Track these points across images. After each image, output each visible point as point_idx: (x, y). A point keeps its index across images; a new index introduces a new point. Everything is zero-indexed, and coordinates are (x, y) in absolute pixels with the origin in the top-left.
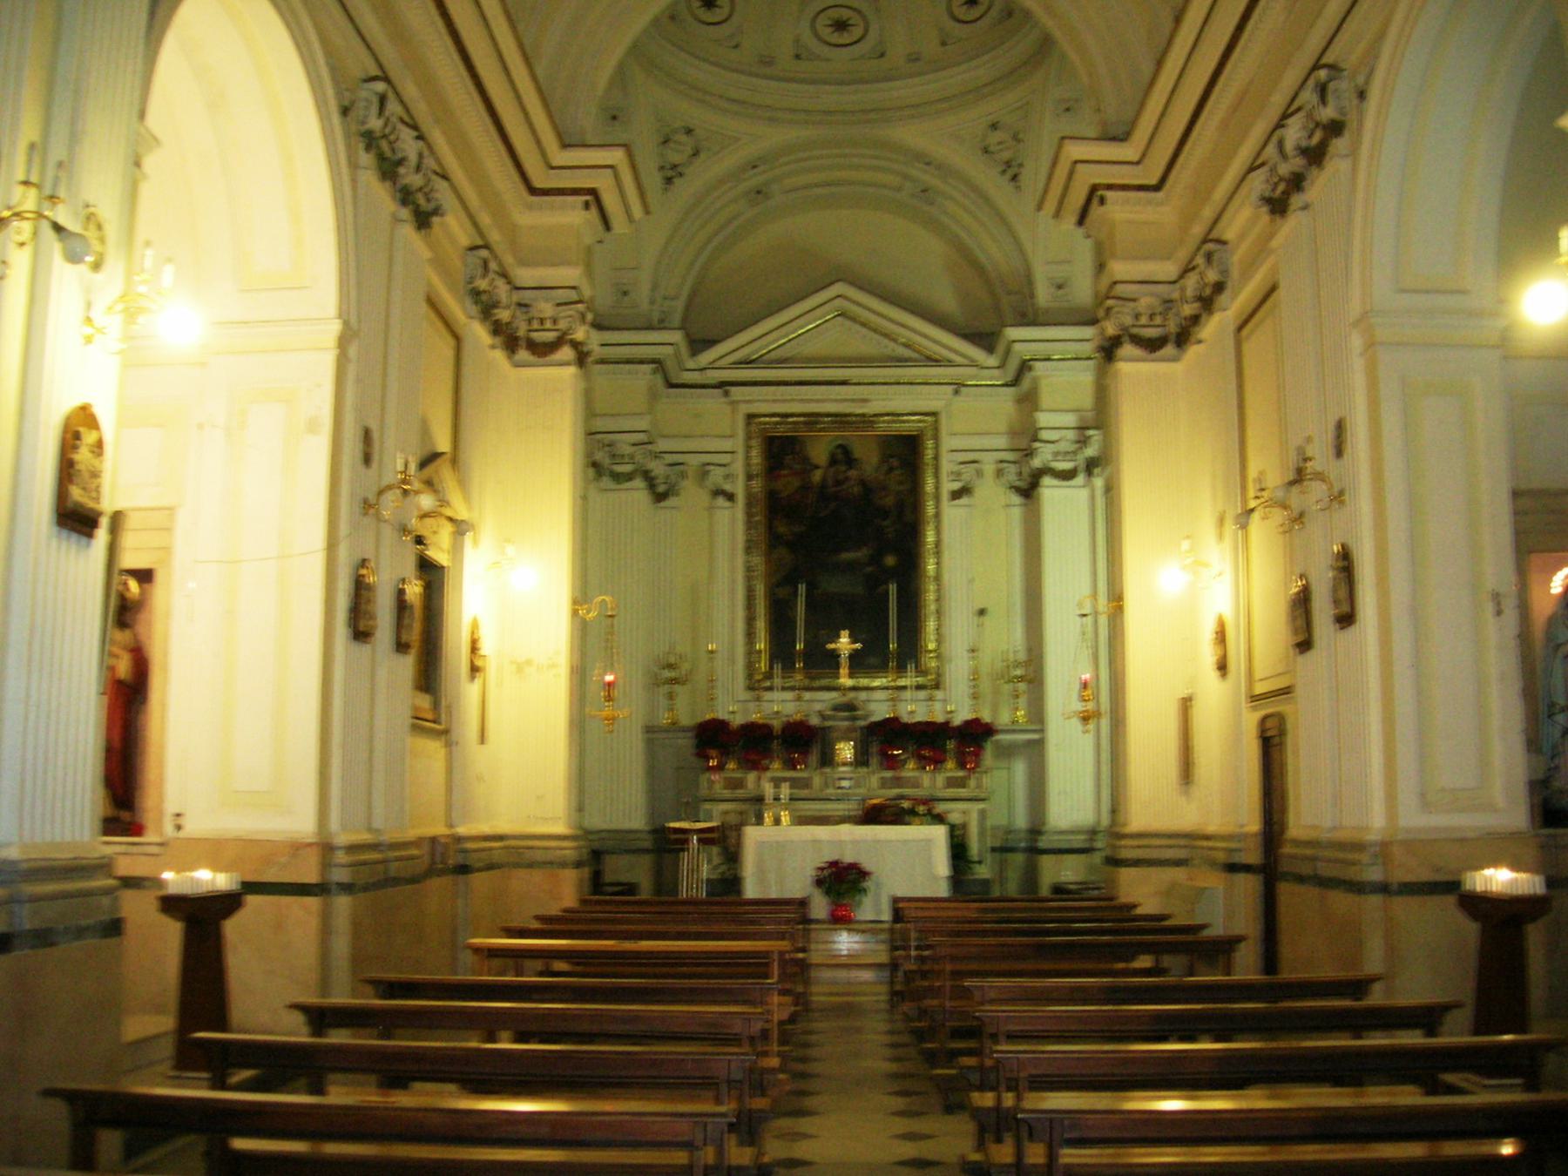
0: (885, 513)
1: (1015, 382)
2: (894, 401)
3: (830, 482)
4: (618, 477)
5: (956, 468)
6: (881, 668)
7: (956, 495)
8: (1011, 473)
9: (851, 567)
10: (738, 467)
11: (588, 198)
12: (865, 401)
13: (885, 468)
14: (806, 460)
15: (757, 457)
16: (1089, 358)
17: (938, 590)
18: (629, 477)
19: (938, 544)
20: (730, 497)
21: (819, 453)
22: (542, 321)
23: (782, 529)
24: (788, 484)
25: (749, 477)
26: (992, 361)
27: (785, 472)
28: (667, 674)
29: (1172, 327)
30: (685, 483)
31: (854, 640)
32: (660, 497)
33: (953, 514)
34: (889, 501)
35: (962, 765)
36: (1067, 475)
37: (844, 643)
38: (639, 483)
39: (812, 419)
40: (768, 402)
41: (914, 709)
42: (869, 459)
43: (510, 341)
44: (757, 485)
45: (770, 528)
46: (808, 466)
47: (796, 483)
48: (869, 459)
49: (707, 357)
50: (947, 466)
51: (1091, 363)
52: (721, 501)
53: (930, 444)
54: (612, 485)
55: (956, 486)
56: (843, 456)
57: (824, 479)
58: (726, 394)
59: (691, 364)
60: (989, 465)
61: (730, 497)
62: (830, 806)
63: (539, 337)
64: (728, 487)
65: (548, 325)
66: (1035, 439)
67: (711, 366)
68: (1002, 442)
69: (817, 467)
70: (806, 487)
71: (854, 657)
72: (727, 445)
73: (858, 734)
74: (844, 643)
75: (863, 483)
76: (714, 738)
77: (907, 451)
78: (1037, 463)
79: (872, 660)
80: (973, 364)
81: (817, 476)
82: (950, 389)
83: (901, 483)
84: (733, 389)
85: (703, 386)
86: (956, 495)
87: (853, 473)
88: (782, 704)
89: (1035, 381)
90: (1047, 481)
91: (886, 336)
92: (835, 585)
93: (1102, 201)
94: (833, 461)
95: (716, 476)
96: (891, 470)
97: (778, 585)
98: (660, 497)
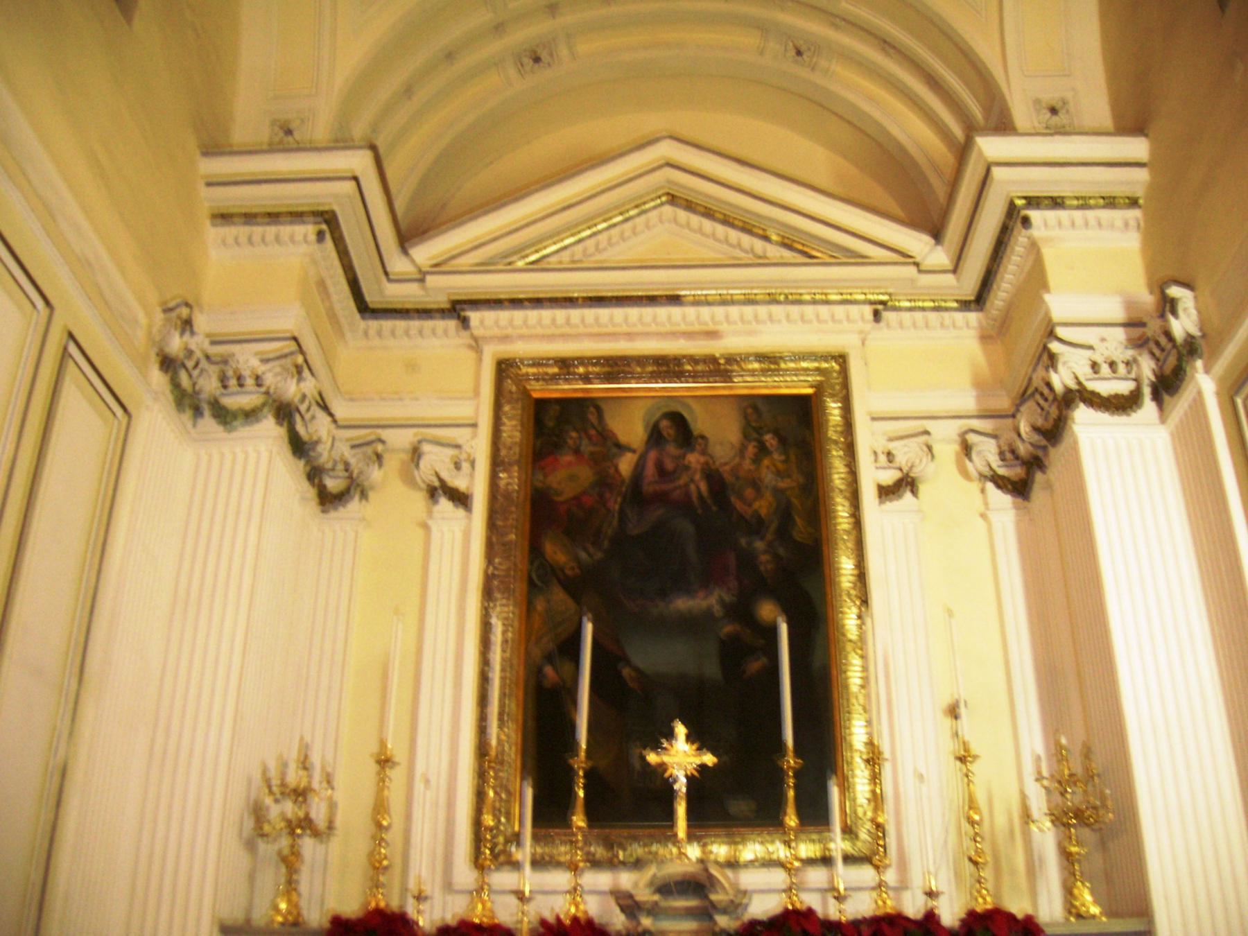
0: (756, 526)
1: (979, 301)
2: (771, 331)
3: (650, 470)
4: (224, 416)
5: (882, 445)
6: (766, 817)
7: (887, 492)
8: (988, 453)
9: (692, 625)
10: (480, 447)
12: (712, 334)
13: (751, 449)
15: (513, 431)
16: (1133, 203)
17: (865, 669)
18: (250, 415)
19: (861, 576)
21: (631, 429)
23: (556, 552)
24: (569, 477)
25: (497, 463)
26: (939, 257)
30: (376, 474)
31: (698, 737)
32: (328, 500)
34: (763, 506)
36: (1123, 405)
37: (681, 756)
38: (269, 430)
39: (616, 367)
40: (538, 337)
42: (722, 435)
43: (188, 402)
44: (511, 480)
45: (535, 550)
46: (612, 445)
47: (586, 475)
48: (722, 435)
49: (425, 253)
50: (867, 438)
51: (1134, 214)
52: (445, 504)
53: (834, 409)
55: (889, 477)
56: (674, 428)
57: (639, 468)
58: (465, 322)
60: (945, 435)
61: (461, 499)
64: (460, 483)
66: (1051, 334)
67: (439, 267)
68: (968, 402)
70: (605, 482)
71: (700, 781)
72: (464, 411)
74: (681, 756)
75: (713, 476)
77: (796, 426)
78: (1060, 380)
79: (739, 806)
81: (625, 465)
84: (474, 316)
85: (425, 313)
86: (887, 492)
87: (693, 459)
89: (1034, 246)
90: (1082, 415)
92: (652, 657)
93: (1026, 222)
94: (655, 437)
95: (436, 461)
97: (549, 658)
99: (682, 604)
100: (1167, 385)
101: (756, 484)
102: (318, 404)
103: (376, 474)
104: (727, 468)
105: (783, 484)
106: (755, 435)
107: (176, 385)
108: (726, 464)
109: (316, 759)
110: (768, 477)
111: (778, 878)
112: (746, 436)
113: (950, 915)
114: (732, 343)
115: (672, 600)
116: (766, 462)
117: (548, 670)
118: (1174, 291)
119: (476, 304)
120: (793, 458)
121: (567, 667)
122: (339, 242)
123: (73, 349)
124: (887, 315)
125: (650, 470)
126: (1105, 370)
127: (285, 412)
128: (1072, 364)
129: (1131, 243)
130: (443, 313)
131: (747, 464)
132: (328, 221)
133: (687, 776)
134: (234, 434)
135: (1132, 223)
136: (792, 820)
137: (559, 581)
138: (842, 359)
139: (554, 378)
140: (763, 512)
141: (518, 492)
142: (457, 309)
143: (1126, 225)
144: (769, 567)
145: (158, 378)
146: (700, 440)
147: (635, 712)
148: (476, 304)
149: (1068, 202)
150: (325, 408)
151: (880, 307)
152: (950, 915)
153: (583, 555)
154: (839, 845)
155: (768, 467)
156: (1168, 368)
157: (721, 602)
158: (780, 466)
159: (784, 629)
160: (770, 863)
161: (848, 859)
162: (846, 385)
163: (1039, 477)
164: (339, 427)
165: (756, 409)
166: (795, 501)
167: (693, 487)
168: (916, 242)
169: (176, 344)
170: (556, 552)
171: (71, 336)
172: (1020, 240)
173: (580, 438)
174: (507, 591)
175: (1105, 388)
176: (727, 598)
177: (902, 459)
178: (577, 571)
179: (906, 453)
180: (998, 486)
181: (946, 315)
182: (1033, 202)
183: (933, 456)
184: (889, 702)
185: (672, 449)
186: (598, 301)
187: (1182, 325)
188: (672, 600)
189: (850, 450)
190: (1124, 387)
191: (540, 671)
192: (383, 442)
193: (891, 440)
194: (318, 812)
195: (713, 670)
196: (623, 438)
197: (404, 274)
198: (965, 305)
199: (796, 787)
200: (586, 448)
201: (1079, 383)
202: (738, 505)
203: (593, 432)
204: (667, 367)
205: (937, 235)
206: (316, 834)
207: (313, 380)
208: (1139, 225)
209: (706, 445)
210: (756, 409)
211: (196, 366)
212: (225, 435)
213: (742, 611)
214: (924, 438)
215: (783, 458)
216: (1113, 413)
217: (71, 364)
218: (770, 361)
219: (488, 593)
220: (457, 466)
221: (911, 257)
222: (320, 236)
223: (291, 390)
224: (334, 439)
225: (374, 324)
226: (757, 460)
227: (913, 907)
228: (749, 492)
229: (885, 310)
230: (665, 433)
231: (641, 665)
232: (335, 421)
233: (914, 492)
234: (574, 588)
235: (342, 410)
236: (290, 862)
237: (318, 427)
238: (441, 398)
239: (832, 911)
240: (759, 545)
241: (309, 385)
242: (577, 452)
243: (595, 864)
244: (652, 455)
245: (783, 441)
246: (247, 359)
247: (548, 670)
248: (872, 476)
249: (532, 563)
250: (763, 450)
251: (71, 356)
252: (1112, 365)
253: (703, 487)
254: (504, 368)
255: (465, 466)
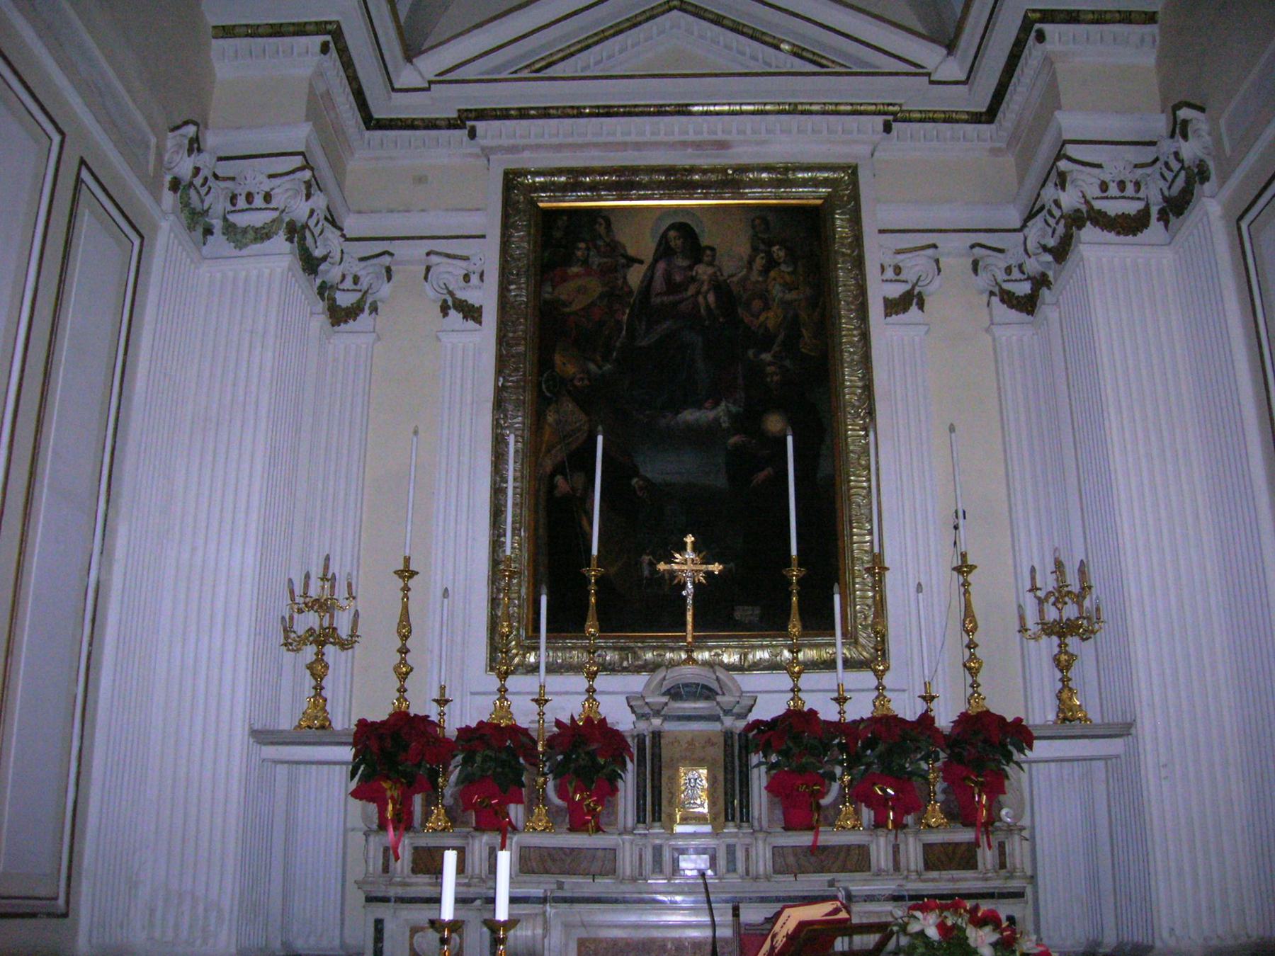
0: (765, 341)
3: (659, 283)
5: (890, 260)
6: (772, 623)
9: (703, 438)
10: (488, 255)
11: (328, 38)
12: (722, 145)
13: (759, 262)
14: (614, 248)
15: (522, 242)
16: (1150, 18)
18: (263, 234)
19: (868, 388)
20: (472, 313)
21: (642, 244)
22: (249, 197)
23: (565, 364)
24: (579, 289)
26: (953, 69)
27: (575, 269)
28: (311, 620)
29: (1154, 193)
31: (706, 550)
32: (339, 316)
33: (887, 336)
34: (771, 318)
35: (961, 813)
36: (1131, 225)
37: (688, 565)
39: (626, 180)
40: (545, 147)
41: (837, 693)
42: (732, 252)
44: (520, 294)
45: (544, 363)
46: (620, 260)
47: (595, 287)
48: (732, 252)
49: (430, 64)
50: (876, 252)
53: (840, 222)
54: (228, 248)
55: (895, 291)
57: (649, 280)
58: (472, 134)
59: (406, 76)
61: (472, 313)
62: (465, 497)
63: (241, 220)
64: (472, 296)
65: (259, 201)
67: (443, 78)
69: (632, 261)
70: (614, 295)
72: (471, 222)
73: (718, 752)
74: (688, 565)
75: (720, 287)
76: (396, 757)
80: (918, 70)
81: (635, 277)
82: (879, 120)
83: (789, 287)
84: (481, 126)
85: (431, 125)
86: (896, 306)
87: (703, 271)
88: (555, 693)
89: (1048, 61)
91: (755, 36)
92: (661, 468)
93: (1041, 37)
94: (664, 250)
95: (449, 273)
96: (771, 264)
97: (559, 469)
98: (339, 316)
99: (689, 416)
100: (1176, 206)
101: (764, 297)
102: (326, 219)
103: (385, 290)
104: (735, 279)
105: (789, 296)
106: (762, 247)
107: (186, 204)
108: (732, 276)
109: (334, 568)
110: (776, 291)
111: (782, 681)
112: (755, 249)
113: (944, 719)
114: (742, 154)
115: (682, 414)
116: (772, 274)
117: (559, 479)
118: (1184, 113)
119: (482, 115)
120: (800, 270)
121: (579, 479)
122: (343, 52)
123: (85, 175)
124: (896, 126)
125: (659, 283)
126: (1113, 190)
127: (295, 231)
128: (1080, 183)
129: (1148, 59)
130: (451, 125)
131: (755, 276)
132: (334, 37)
133: (693, 583)
134: (246, 251)
135: (1148, 39)
136: (795, 627)
137: (569, 392)
138: (853, 171)
139: (564, 189)
140: (771, 324)
141: (526, 303)
142: (465, 120)
143: (1142, 40)
144: (775, 378)
145: (169, 198)
146: (708, 252)
147: (646, 520)
148: (482, 115)
149: (1082, 17)
150: (333, 223)
151: (891, 118)
152: (944, 719)
153: (592, 367)
154: (841, 651)
155: (774, 279)
156: (1175, 191)
157: (729, 412)
158: (788, 278)
159: (790, 439)
160: (773, 666)
161: (849, 664)
162: (855, 196)
163: (1045, 292)
164: (347, 240)
165: (764, 220)
166: (803, 315)
167: (701, 299)
168: (929, 55)
169: (184, 166)
170: (565, 364)
171: (83, 162)
172: (1033, 54)
173: (588, 249)
174: (519, 404)
175: (1113, 208)
176: (734, 409)
177: (909, 275)
178: (586, 382)
179: (915, 266)
180: (1003, 301)
181: (956, 126)
182: (1050, 16)
183: (939, 270)
184: (878, 469)
185: (681, 262)
186: (607, 112)
187: (1190, 150)
188: (682, 414)
189: (859, 263)
190: (1132, 208)
191: (552, 487)
192: (391, 255)
193: (898, 252)
194: (343, 625)
195: (720, 481)
196: (631, 251)
197: (415, 85)
198: (976, 118)
199: (799, 593)
200: (596, 261)
201: (1087, 202)
202: (747, 319)
203: (600, 243)
204: (677, 180)
205: (951, 47)
206: (345, 645)
207: (321, 195)
208: (1154, 41)
209: (714, 256)
210: (764, 220)
211: (203, 185)
212: (236, 252)
213: (749, 420)
214: (930, 252)
215: (790, 269)
216: (1118, 233)
217: (84, 187)
218: (783, 175)
219: (499, 404)
220: (467, 278)
221: (922, 67)
222: (325, 48)
223: (300, 210)
224: (342, 252)
225: (378, 134)
226: (766, 271)
227: (907, 708)
228: (757, 304)
229: (895, 121)
230: (672, 244)
231: (649, 475)
232: (343, 236)
233: (921, 306)
234: (585, 400)
235: (352, 225)
236: (318, 670)
237: (327, 243)
238: (447, 208)
239: (828, 712)
240: (766, 357)
241: (319, 201)
242: (585, 262)
243: (610, 669)
244: (661, 266)
245: (792, 258)
246: (254, 177)
247: (559, 479)
248: (879, 290)
249: (540, 374)
250: (771, 264)
251: (83, 181)
252: (1122, 185)
253: (711, 298)
254: (511, 180)
255: (475, 279)
